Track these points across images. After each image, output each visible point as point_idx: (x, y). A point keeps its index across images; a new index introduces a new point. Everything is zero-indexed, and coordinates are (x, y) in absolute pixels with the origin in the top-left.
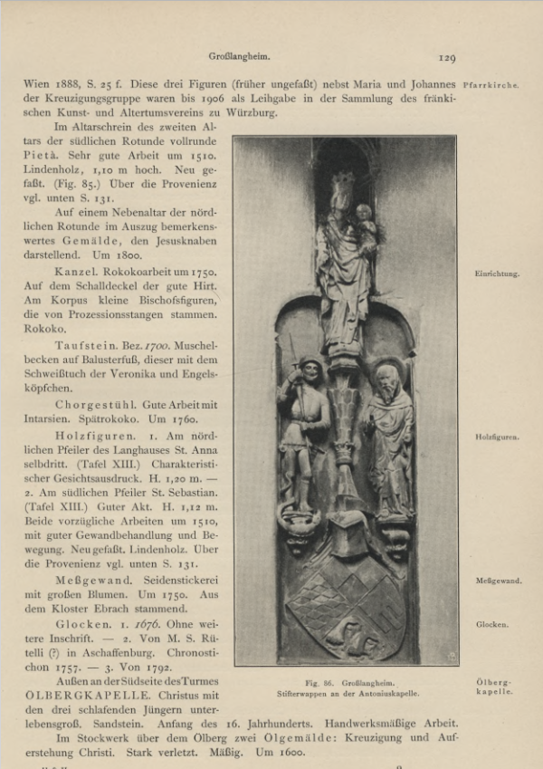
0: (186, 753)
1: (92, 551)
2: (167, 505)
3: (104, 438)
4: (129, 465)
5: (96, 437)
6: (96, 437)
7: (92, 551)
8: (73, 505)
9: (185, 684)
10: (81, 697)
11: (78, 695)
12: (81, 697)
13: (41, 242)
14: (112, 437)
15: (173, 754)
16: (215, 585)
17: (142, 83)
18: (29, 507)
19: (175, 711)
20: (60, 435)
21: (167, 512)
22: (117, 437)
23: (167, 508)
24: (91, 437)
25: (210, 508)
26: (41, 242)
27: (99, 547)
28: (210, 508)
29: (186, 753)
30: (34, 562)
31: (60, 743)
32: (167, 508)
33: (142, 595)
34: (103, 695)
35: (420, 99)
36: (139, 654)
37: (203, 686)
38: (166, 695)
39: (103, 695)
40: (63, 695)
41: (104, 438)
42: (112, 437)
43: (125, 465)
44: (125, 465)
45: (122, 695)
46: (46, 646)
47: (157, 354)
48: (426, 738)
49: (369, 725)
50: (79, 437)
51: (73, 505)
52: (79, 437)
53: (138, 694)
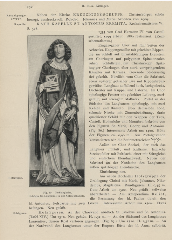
2: (149, 184)
5: (52, 213)
6: (52, 213)
9: (98, 24)
10: (92, 15)
11: (92, 14)
12: (92, 15)
13: (102, 117)
14: (57, 213)
15: (75, 222)
18: (30, 217)
20: (40, 212)
21: (149, 187)
23: (149, 186)
24: (50, 213)
25: (163, 185)
26: (102, 117)
27: (78, 216)
28: (163, 185)
30: (93, 198)
31: (108, 132)
32: (149, 186)
34: (58, 24)
37: (139, 56)
38: (134, 63)
39: (58, 24)
40: (109, 23)
41: (54, 213)
42: (57, 213)
45: (63, 24)
46: (126, 224)
49: (137, 99)
50: (46, 213)
52: (46, 213)
53: (69, 23)
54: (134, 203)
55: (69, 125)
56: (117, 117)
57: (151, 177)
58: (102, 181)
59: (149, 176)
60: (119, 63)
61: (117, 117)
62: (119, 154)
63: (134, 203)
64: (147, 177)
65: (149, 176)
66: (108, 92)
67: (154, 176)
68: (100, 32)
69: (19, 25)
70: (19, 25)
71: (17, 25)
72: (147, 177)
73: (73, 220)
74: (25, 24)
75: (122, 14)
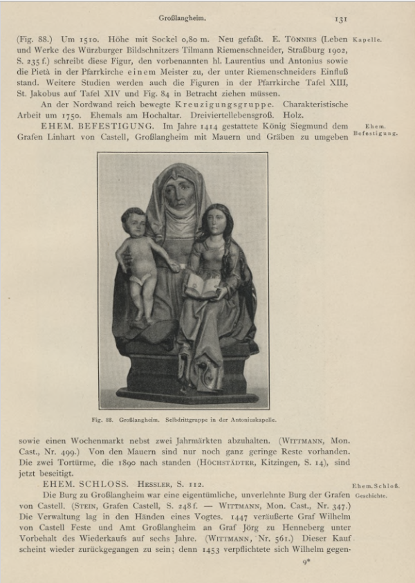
0: (28, 474)
1: (227, 105)
3: (214, 106)
4: (343, 83)
7: (227, 105)
8: (340, 81)
10: (127, 127)
12: (127, 127)
13: (221, 116)
15: (262, 496)
16: (323, 86)
17: (311, 537)
19: (151, 452)
22: (187, 105)
26: (221, 116)
29: (28, 474)
33: (64, 40)
35: (328, 82)
36: (105, 51)
41: (214, 106)
43: (340, 84)
44: (340, 84)
47: (138, 447)
48: (204, 137)
51: (340, 81)
54: (292, 137)
55: (169, 191)
56: (34, 83)
57: (254, 105)
58: (123, 62)
59: (248, 105)
60: (217, 83)
61: (34, 83)
62: (85, 73)
63: (292, 137)
64: (243, 106)
65: (248, 105)
66: (177, 97)
67: (261, 105)
68: (339, 20)
69: (365, 40)
70: (365, 40)
71: (360, 40)
72: (243, 106)
73: (259, 493)
74: (378, 40)
75: (278, 39)
